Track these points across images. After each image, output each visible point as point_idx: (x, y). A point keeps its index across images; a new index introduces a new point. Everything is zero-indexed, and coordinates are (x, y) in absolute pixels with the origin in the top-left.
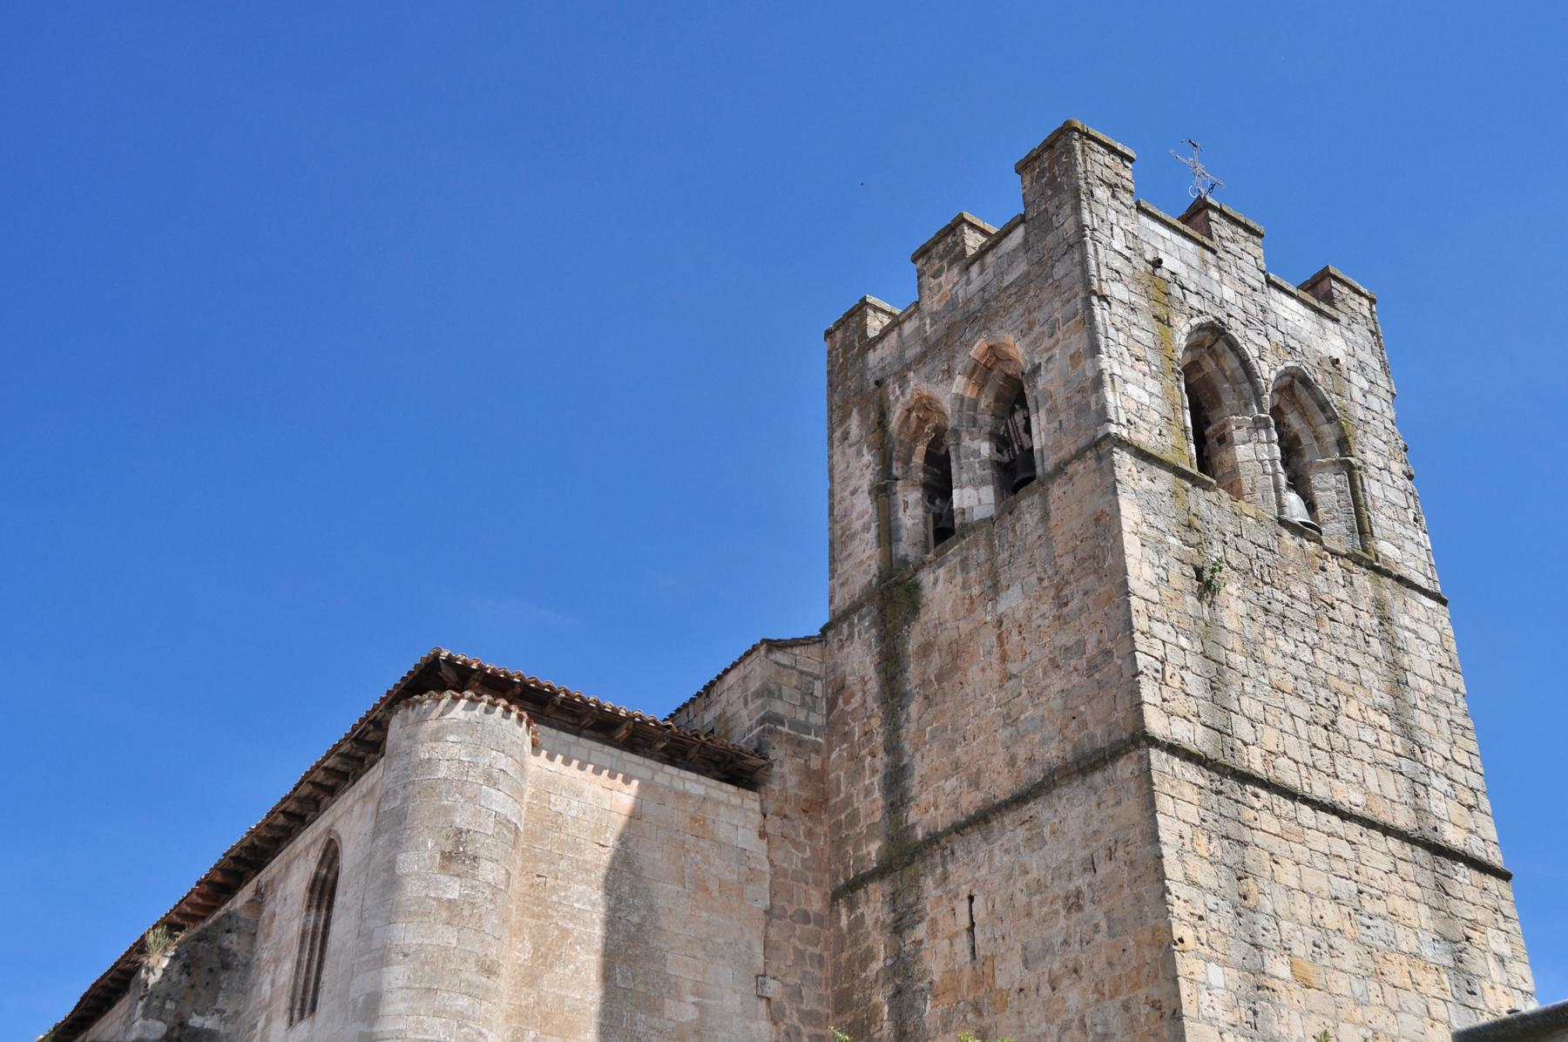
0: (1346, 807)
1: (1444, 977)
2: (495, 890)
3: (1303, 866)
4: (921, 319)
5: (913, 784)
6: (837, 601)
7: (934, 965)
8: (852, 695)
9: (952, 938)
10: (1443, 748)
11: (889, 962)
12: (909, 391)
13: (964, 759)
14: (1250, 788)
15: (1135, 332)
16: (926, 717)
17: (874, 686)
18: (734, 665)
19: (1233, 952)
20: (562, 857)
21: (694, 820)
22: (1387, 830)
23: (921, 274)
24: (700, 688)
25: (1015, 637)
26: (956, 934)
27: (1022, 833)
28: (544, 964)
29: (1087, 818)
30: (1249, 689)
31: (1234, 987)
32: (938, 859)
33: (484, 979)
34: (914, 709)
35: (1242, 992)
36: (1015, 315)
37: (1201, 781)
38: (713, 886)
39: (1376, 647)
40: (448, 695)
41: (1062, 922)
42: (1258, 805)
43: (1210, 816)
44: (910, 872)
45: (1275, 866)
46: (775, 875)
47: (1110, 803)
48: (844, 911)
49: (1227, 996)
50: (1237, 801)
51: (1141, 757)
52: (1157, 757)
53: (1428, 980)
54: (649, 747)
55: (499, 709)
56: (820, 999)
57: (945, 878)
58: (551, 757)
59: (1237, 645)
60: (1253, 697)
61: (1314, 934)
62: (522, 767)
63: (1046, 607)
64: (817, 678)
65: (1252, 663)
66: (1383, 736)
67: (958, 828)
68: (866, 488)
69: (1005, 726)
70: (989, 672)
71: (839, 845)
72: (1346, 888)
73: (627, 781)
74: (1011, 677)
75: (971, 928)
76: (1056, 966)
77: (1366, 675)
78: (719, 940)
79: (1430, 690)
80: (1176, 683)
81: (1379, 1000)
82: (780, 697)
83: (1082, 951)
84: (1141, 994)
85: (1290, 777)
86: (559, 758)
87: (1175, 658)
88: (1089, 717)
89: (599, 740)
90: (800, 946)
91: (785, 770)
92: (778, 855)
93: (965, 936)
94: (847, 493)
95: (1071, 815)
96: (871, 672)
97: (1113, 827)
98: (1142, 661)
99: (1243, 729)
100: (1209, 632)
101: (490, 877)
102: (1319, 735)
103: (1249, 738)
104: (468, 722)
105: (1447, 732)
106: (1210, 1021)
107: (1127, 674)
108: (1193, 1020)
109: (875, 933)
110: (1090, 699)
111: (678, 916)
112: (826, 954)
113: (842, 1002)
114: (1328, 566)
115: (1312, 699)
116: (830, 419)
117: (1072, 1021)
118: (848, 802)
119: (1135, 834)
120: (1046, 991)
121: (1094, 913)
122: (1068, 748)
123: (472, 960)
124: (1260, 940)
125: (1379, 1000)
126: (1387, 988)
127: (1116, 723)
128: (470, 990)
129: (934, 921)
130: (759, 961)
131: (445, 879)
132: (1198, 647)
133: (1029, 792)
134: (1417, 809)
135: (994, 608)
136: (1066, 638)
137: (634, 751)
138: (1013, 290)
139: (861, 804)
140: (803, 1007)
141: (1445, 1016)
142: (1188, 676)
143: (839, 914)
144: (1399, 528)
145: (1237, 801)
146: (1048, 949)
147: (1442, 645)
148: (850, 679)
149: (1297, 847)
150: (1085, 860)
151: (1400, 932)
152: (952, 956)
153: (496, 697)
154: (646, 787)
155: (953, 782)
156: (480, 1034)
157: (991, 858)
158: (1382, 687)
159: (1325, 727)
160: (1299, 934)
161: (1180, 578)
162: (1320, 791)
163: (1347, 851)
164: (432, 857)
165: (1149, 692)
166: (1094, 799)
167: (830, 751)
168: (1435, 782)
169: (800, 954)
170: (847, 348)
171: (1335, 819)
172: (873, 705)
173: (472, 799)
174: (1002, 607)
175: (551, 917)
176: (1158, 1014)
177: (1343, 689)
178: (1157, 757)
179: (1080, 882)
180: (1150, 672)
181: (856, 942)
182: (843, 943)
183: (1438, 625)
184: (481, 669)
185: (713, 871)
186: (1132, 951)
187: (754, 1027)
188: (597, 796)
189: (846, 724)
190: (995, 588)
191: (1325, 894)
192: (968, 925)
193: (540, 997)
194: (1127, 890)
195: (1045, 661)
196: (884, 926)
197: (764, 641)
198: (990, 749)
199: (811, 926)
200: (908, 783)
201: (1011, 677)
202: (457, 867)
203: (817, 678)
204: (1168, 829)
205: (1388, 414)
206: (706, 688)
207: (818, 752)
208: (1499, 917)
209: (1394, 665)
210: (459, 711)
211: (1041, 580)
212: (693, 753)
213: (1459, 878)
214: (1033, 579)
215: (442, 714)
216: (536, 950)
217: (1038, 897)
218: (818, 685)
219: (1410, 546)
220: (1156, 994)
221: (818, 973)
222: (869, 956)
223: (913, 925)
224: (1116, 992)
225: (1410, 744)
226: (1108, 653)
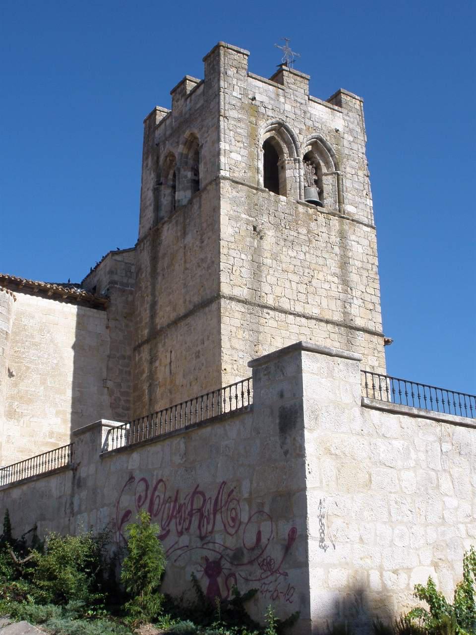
4: (172, 119)
5: (158, 307)
6: (140, 234)
8: (143, 273)
9: (165, 367)
10: (363, 288)
11: (148, 374)
12: (166, 149)
13: (172, 300)
14: (265, 310)
15: (239, 130)
17: (149, 269)
23: (173, 100)
36: (199, 121)
37: (243, 310)
39: (337, 249)
43: (245, 323)
48: (137, 355)
63: (198, 243)
64: (133, 265)
66: (333, 286)
67: (169, 326)
68: (152, 188)
75: (170, 363)
77: (329, 262)
82: (116, 274)
85: (286, 306)
87: (238, 263)
90: (121, 368)
94: (146, 190)
100: (257, 252)
105: (365, 281)
114: (319, 219)
116: (143, 157)
129: (161, 360)
130: (105, 375)
135: (184, 242)
138: (198, 111)
140: (122, 390)
142: (243, 270)
143: (136, 356)
144: (357, 199)
148: (143, 266)
157: (177, 337)
158: (337, 266)
161: (246, 230)
162: (299, 309)
170: (150, 127)
171: (303, 320)
172: (148, 276)
175: (23, 363)
179: (199, 348)
183: (369, 238)
189: (141, 283)
190: (185, 234)
193: (19, 391)
197: (111, 252)
200: (156, 307)
201: (186, 269)
203: (133, 265)
205: (361, 150)
208: (376, 352)
211: (197, 231)
212: (78, 299)
214: (195, 231)
218: (133, 267)
219: (361, 206)
222: (143, 372)
223: (156, 360)
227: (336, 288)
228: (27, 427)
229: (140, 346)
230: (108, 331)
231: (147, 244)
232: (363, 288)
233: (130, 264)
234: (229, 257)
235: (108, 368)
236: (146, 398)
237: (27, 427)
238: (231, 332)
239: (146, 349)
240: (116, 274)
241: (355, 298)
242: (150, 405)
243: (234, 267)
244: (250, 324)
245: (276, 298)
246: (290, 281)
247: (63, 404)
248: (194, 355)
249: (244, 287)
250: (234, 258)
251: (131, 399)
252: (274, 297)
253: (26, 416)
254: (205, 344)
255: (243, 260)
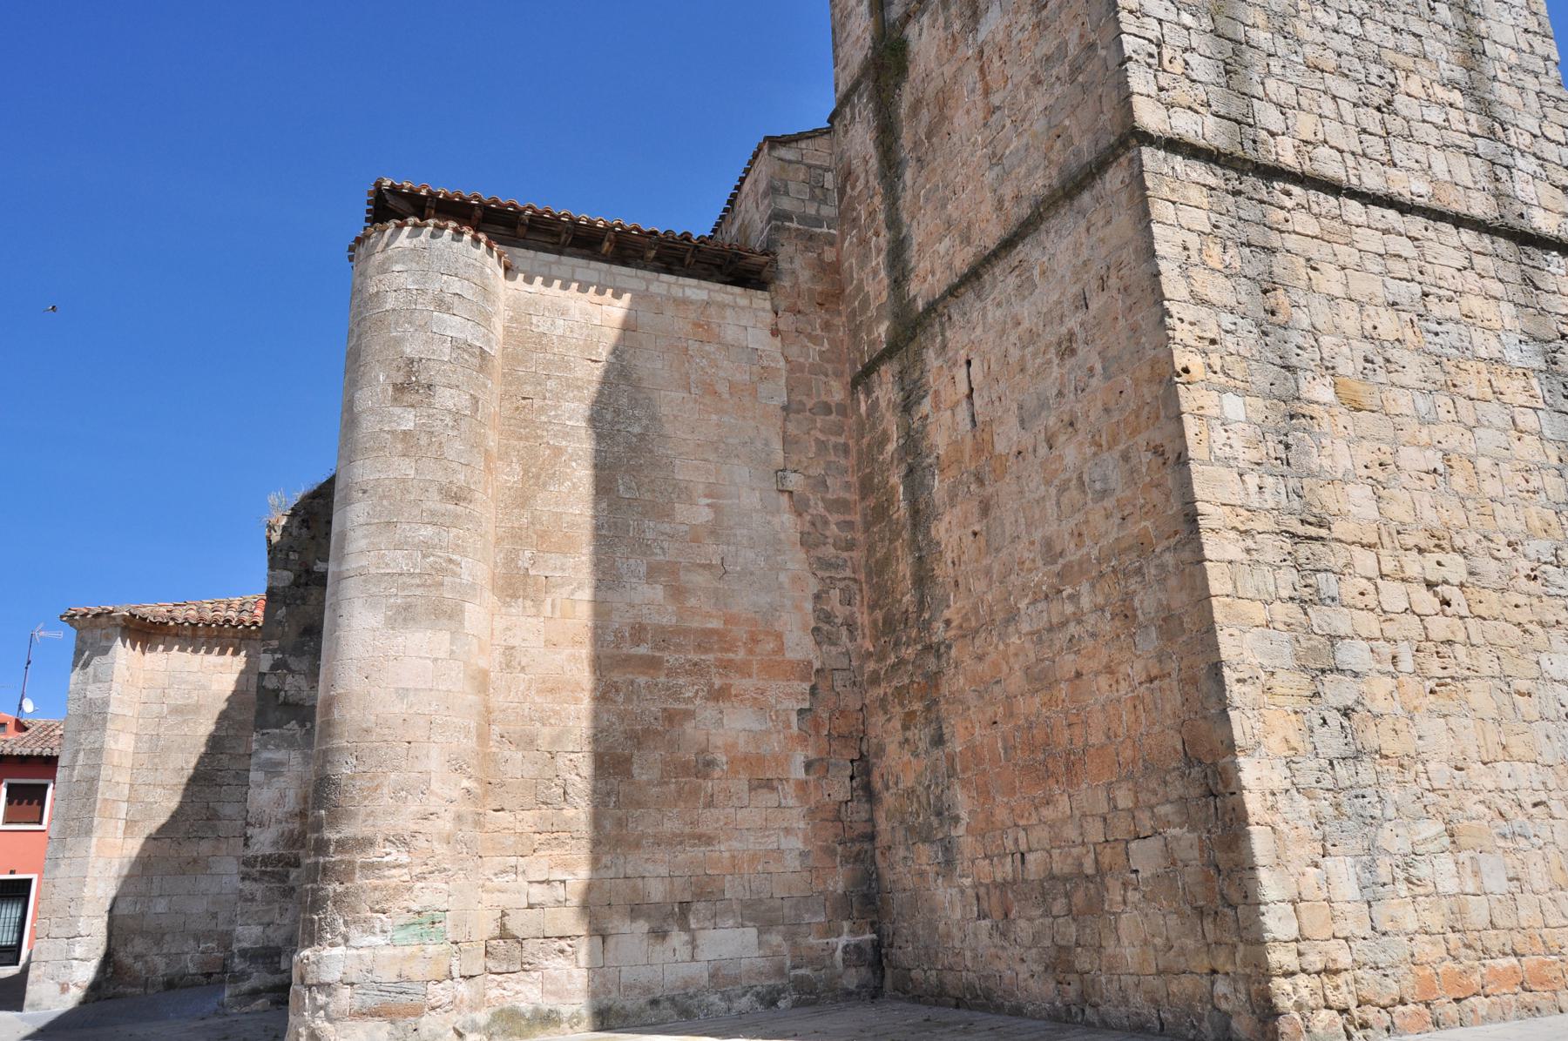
0: (1407, 197)
1: (1534, 382)
2: (457, 416)
3: (1345, 272)
5: (912, 254)
7: (939, 440)
10: (1531, 124)
11: (901, 441)
13: (955, 215)
16: (921, 180)
17: (874, 163)
18: (747, 171)
19: (1258, 378)
20: (548, 377)
21: (697, 325)
22: (1459, 221)
24: (724, 205)
25: (997, 63)
26: (957, 403)
27: (1012, 280)
28: (536, 484)
29: (1077, 247)
30: (1276, 70)
31: (1259, 418)
32: (937, 328)
33: (451, 507)
34: (908, 176)
35: (1270, 423)
37: (1212, 181)
38: (723, 389)
40: (392, 224)
41: (1056, 371)
42: (1289, 203)
44: (913, 346)
45: (1312, 273)
46: (791, 371)
47: (1101, 223)
48: (862, 397)
49: (1250, 431)
50: (1261, 202)
51: (1131, 160)
52: (1151, 158)
53: (1513, 389)
54: (642, 258)
55: (448, 233)
56: (847, 486)
57: (944, 346)
58: (529, 280)
59: (1261, 19)
60: (1282, 79)
61: (1367, 347)
62: (486, 291)
64: (827, 170)
65: (1280, 41)
67: (953, 291)
69: (992, 166)
70: (973, 113)
71: (855, 333)
72: (1405, 292)
73: (617, 295)
74: (994, 110)
75: (970, 396)
76: (1052, 421)
77: (1431, 46)
78: (731, 441)
79: (1514, 59)
80: (1178, 67)
81: (1452, 416)
82: (787, 193)
83: (1078, 401)
84: (1141, 440)
85: (1329, 165)
86: (539, 280)
87: (1175, 38)
88: (1074, 131)
89: (584, 257)
91: (797, 265)
92: (794, 351)
93: (964, 404)
95: (1061, 249)
96: (871, 149)
97: (1103, 252)
98: (1129, 44)
99: (1269, 117)
101: (450, 404)
102: (1371, 119)
103: (1277, 127)
104: (414, 249)
105: (1535, 105)
106: (1226, 462)
107: (1112, 64)
108: (1203, 463)
109: (888, 415)
110: (1074, 108)
111: (683, 422)
112: (851, 443)
113: (866, 487)
115: (1362, 77)
117: (1070, 480)
118: (860, 288)
119: (1128, 255)
120: (1043, 450)
121: (1088, 355)
122: (1054, 173)
123: (433, 489)
124: (1294, 361)
125: (1452, 416)
126: (1461, 402)
127: (1104, 128)
128: (434, 519)
130: (779, 457)
131: (398, 410)
132: (1206, 23)
133: (1016, 234)
134: (1498, 195)
135: (974, 39)
136: (1047, 46)
137: (625, 263)
139: (870, 288)
140: (829, 496)
141: (1536, 426)
145: (1261, 202)
146: (1043, 405)
147: (1528, 7)
149: (1342, 250)
150: (1076, 296)
151: (1478, 337)
152: (954, 427)
153: (461, 224)
154: (640, 298)
155: (947, 242)
156: (450, 561)
157: (984, 316)
158: (1453, 58)
159: (1379, 109)
160: (1345, 350)
162: (1372, 181)
163: (1407, 248)
164: (384, 391)
165: (1139, 80)
166: (1083, 224)
167: (843, 241)
168: (1521, 162)
169: (822, 446)
171: (1392, 215)
172: (874, 182)
173: (424, 327)
174: (983, 33)
176: (1161, 460)
177: (1401, 64)
178: (1151, 158)
179: (1072, 323)
180: (1142, 58)
181: (873, 427)
182: (863, 428)
184: (432, 195)
185: (722, 374)
186: (1129, 391)
187: (776, 520)
188: (585, 313)
189: (854, 209)
191: (1379, 301)
192: (966, 391)
193: (533, 517)
194: (1122, 322)
195: (1027, 81)
196: (895, 406)
197: (767, 138)
198: (978, 197)
199: (833, 417)
201: (994, 110)
202: (410, 398)
203: (827, 170)
204: (1166, 241)
206: (729, 202)
207: (832, 244)
209: (1467, 33)
210: (404, 240)
213: (1553, 269)
215: (387, 245)
216: (526, 472)
217: (1031, 349)
218: (829, 177)
220: (1157, 437)
221: (843, 462)
222: (884, 439)
224: (1114, 441)
225: (1489, 122)
226: (1092, 46)
227: (1463, 121)
228: (563, 617)
229: (869, 370)
230: (777, 341)
231: (864, 108)
232: (1531, 124)
233: (820, 167)
234: (1146, 20)
235: (786, 441)
236: (901, 510)
237: (563, 617)
238: (1185, 248)
239: (888, 372)
240: (787, 193)
241: (1517, 153)
242: (915, 526)
243: (1164, 51)
244: (1240, 225)
245: (1303, 148)
246: (1334, 97)
247: (666, 545)
248: (1053, 350)
249: (1201, 109)
250: (1160, 21)
251: (857, 518)
252: (1297, 143)
253: (562, 586)
254: (1093, 306)
255: (1188, 29)
